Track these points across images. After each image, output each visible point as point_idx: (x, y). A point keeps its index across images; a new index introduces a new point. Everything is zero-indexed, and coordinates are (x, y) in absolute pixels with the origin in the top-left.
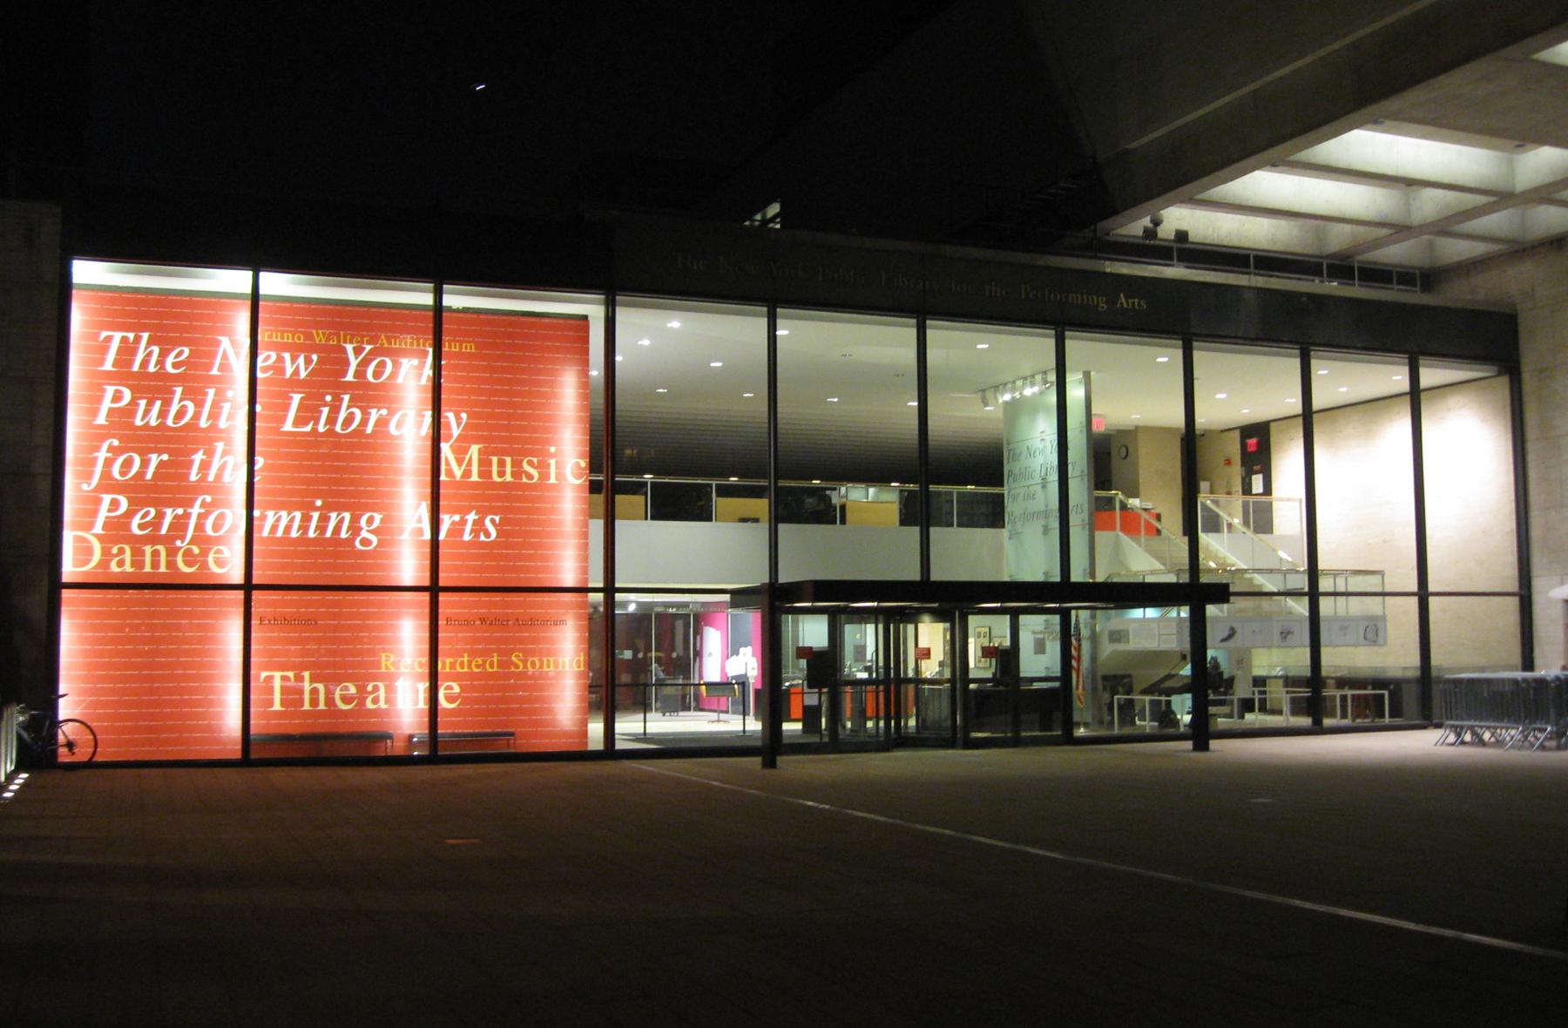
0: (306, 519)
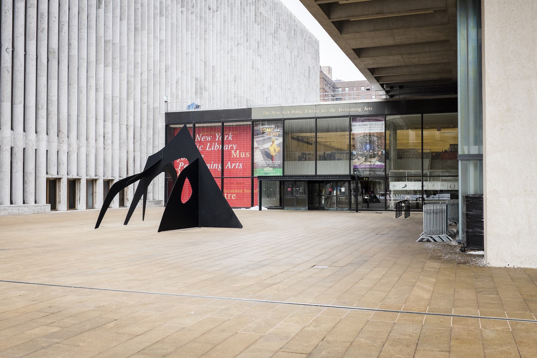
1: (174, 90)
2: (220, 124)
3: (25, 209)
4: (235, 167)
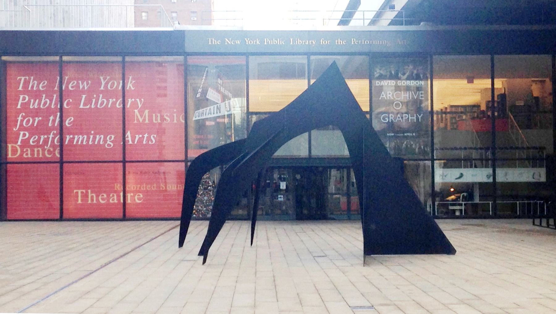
4: (141, 140)
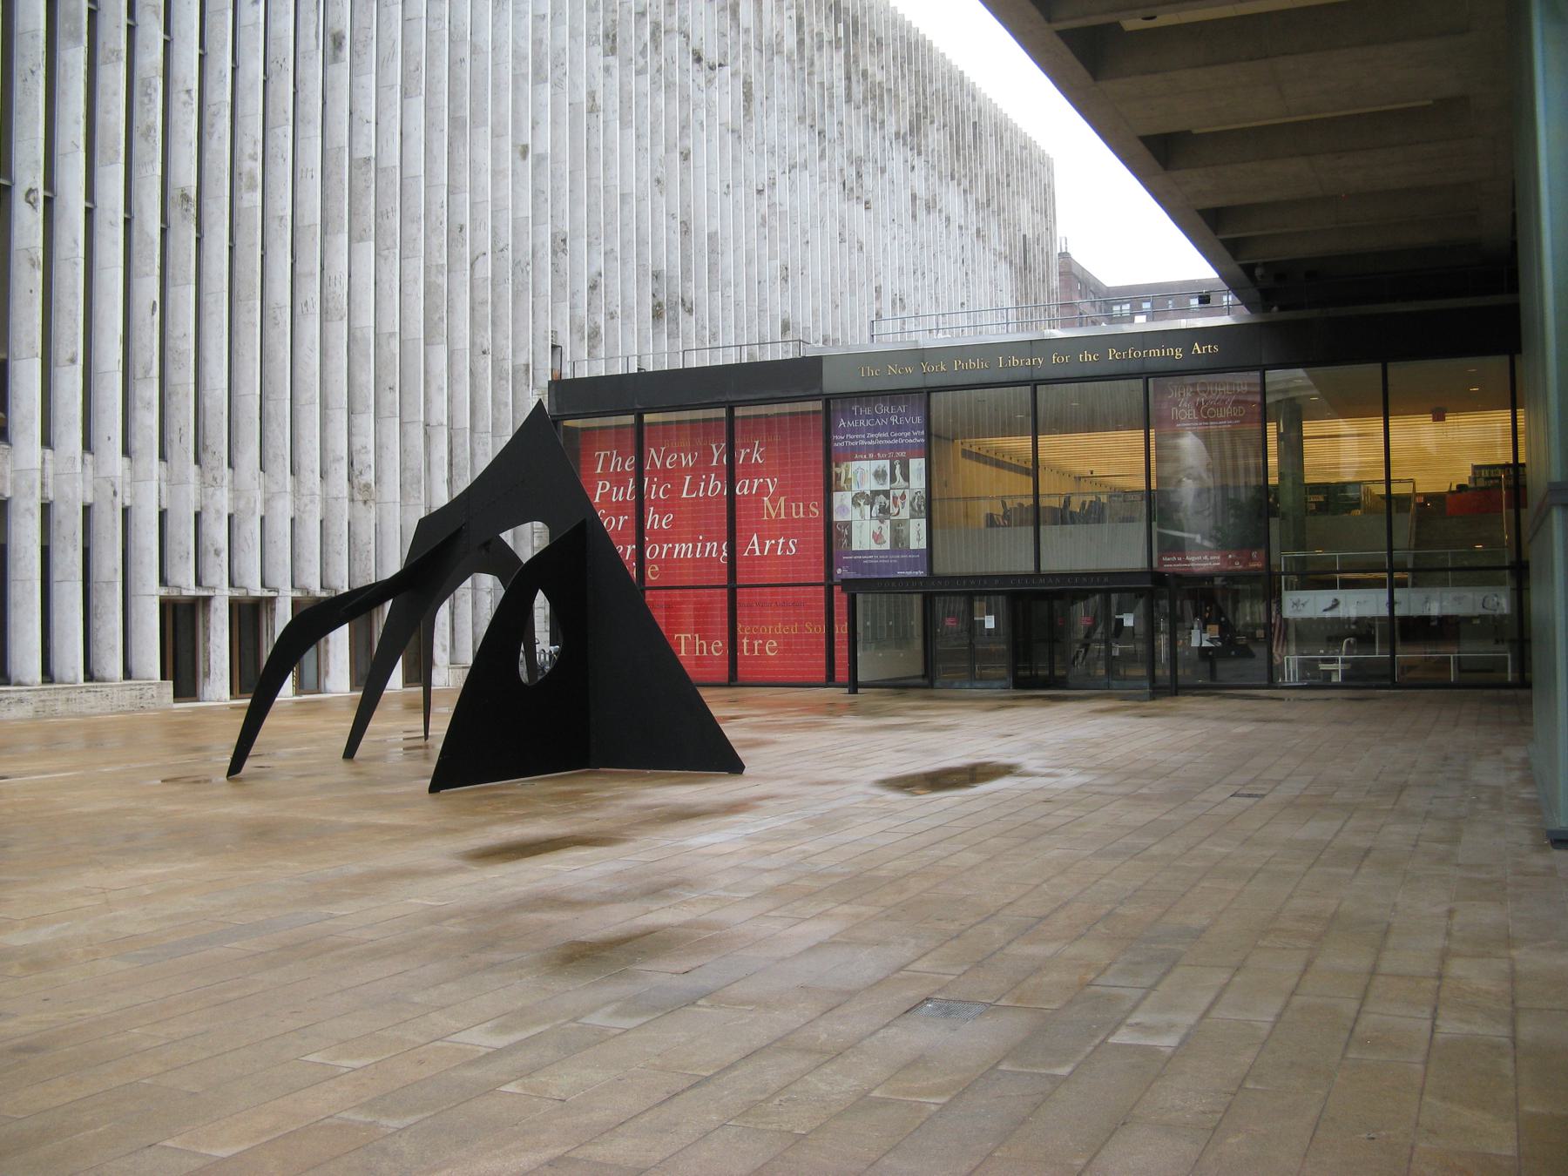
0: (695, 547)
1: (583, 311)
2: (722, 413)
3: (92, 702)
4: (773, 548)
